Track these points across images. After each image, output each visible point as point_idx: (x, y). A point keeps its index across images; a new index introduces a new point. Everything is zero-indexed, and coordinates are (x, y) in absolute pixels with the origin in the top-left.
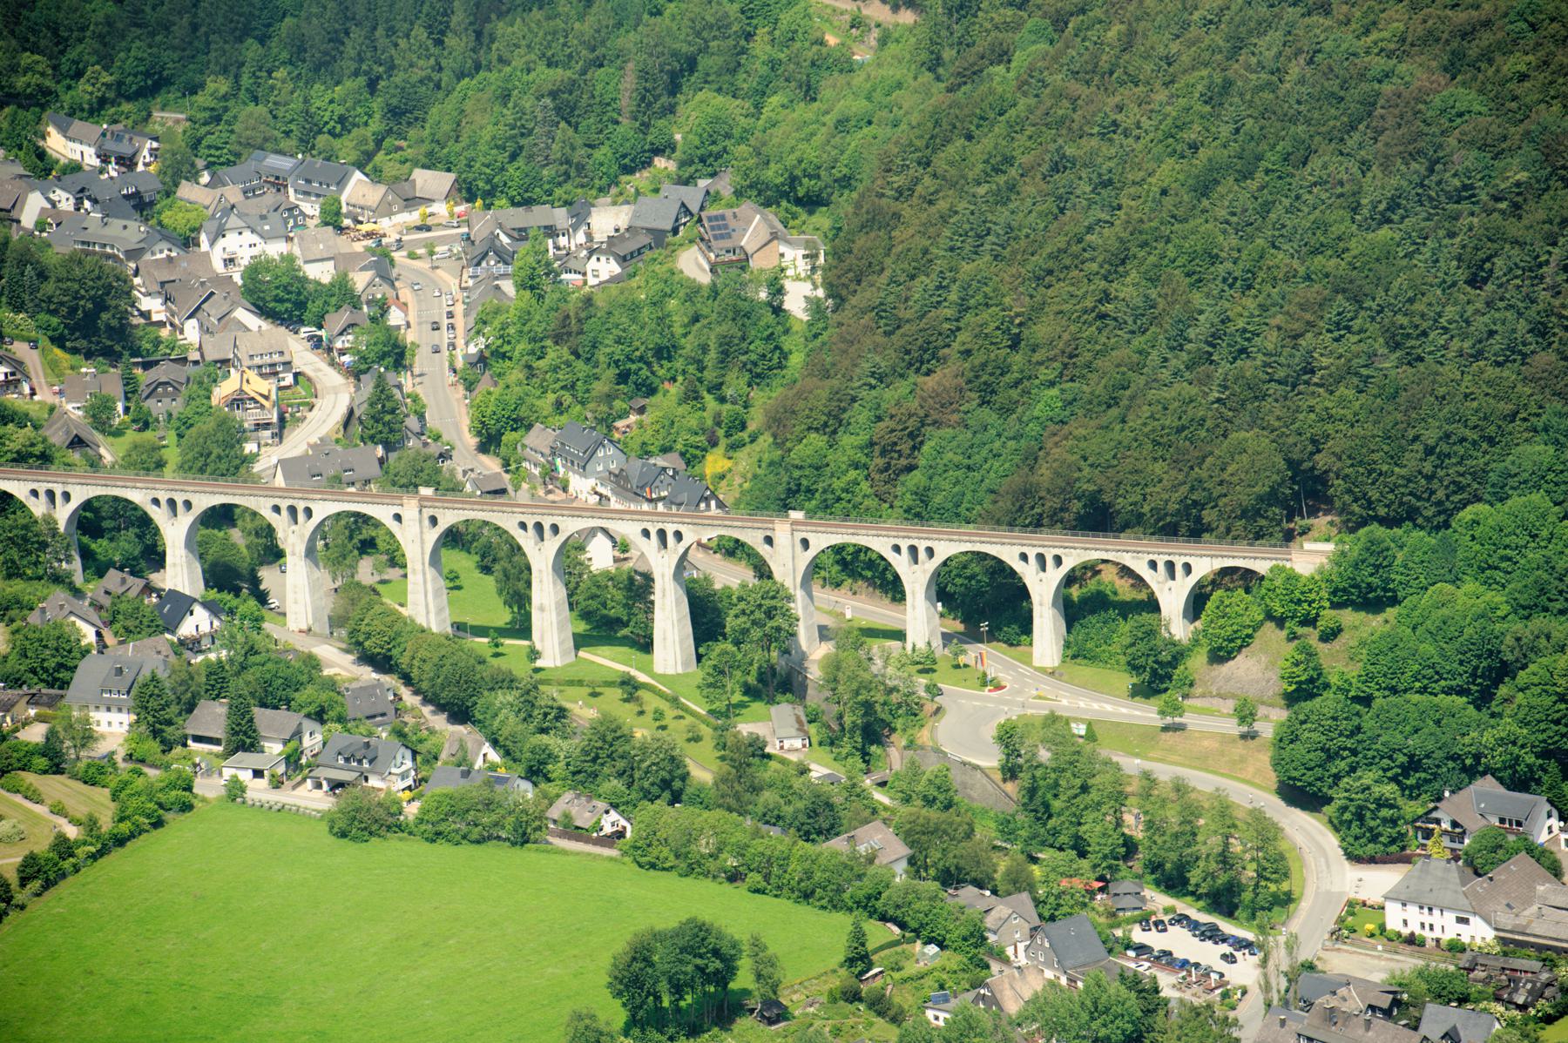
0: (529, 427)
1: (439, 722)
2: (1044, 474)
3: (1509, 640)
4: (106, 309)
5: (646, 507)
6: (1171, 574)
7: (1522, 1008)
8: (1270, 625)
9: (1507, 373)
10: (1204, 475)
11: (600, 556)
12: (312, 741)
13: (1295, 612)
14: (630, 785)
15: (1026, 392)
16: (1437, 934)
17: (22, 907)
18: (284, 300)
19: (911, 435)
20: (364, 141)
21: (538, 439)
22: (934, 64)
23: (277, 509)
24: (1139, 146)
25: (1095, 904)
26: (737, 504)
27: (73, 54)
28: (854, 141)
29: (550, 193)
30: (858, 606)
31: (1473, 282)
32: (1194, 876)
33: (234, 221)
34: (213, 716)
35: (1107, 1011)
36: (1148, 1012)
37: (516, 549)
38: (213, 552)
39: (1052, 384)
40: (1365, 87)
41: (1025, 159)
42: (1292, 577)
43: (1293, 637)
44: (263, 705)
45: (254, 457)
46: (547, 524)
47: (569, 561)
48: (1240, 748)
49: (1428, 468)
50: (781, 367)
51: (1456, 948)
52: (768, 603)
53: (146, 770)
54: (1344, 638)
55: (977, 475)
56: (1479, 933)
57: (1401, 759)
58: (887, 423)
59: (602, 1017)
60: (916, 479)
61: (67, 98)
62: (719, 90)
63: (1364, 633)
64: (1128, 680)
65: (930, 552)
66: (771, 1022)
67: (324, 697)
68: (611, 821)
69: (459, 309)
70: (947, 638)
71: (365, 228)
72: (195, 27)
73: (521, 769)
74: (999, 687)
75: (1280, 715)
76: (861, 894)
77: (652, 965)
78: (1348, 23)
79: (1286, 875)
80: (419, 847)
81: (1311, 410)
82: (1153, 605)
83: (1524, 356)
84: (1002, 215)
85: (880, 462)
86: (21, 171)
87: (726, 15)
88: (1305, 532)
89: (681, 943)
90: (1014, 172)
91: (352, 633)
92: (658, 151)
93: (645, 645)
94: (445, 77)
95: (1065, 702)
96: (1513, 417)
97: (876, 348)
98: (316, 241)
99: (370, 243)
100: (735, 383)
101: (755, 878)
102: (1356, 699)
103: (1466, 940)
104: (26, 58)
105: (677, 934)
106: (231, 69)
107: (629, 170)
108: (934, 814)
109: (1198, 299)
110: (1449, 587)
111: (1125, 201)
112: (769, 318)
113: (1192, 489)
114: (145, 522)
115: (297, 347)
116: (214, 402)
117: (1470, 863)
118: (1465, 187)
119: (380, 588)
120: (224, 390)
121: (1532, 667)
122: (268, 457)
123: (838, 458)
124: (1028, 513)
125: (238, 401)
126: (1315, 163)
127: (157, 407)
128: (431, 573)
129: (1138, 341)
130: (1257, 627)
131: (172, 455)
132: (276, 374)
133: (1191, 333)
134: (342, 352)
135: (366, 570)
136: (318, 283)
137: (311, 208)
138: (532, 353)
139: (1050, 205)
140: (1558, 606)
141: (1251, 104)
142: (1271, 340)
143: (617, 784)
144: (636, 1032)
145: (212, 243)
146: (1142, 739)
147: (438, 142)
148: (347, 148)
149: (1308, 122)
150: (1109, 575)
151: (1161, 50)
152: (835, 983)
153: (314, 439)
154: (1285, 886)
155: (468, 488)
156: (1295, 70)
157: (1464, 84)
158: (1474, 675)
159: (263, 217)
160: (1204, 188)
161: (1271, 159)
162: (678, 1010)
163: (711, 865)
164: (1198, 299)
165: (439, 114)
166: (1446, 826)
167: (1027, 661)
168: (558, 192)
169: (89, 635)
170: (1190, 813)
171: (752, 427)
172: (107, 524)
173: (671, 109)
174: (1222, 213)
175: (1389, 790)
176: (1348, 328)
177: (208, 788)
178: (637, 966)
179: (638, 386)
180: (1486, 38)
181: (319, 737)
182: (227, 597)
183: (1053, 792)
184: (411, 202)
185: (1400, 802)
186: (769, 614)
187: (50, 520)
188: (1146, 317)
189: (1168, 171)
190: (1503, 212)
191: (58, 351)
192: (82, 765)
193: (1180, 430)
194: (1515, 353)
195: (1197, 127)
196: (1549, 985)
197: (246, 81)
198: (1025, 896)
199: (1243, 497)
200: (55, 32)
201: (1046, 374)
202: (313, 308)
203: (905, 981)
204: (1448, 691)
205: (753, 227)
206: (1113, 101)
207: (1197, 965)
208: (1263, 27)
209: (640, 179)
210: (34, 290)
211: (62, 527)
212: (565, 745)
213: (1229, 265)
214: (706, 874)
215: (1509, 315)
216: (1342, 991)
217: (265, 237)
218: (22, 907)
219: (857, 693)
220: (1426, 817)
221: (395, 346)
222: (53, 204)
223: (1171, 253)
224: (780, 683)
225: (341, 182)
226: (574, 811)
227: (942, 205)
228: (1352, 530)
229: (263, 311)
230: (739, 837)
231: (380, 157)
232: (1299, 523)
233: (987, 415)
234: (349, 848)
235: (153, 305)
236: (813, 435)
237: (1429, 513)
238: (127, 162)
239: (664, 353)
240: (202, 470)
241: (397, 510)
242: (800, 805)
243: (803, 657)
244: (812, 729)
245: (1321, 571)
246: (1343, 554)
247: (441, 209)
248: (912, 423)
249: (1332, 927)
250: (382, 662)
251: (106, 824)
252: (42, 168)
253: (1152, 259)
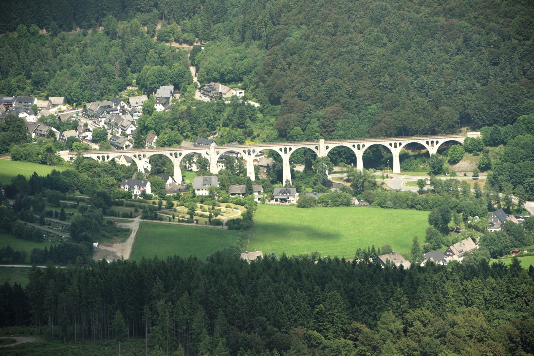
13: (472, 148)
74: (392, 178)
107: (121, 91)
147: (56, 89)
241: (208, 151)
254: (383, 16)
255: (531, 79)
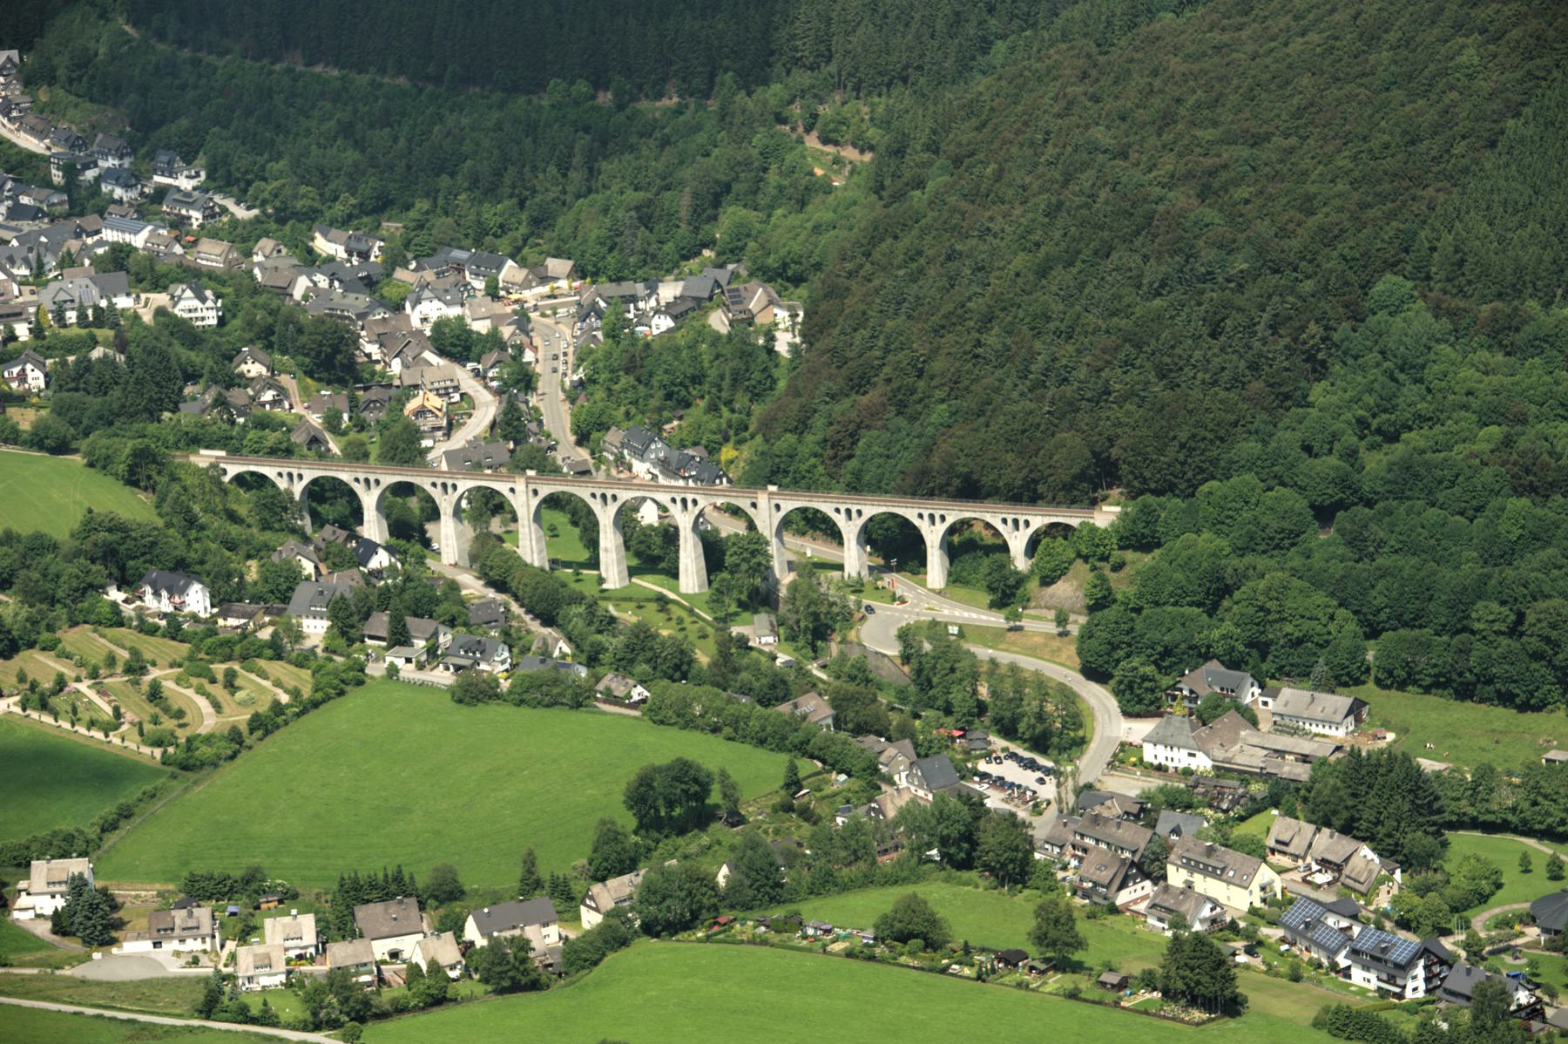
0: (608, 429)
1: (535, 626)
2: (936, 461)
3: (1230, 570)
4: (339, 352)
5: (681, 483)
6: (1017, 528)
7: (1225, 811)
8: (1079, 561)
9: (1233, 395)
10: (1038, 461)
11: (648, 516)
12: (445, 639)
13: (1095, 550)
14: (654, 669)
15: (926, 406)
16: (1175, 764)
17: (250, 748)
18: (455, 343)
19: (851, 435)
20: (516, 240)
21: (613, 437)
22: (878, 189)
23: (434, 485)
24: (1002, 244)
25: (956, 746)
26: (739, 479)
27: (332, 186)
28: (824, 239)
29: (634, 273)
30: (813, 548)
31: (1214, 335)
32: (1022, 727)
33: (427, 293)
34: (381, 622)
35: (949, 818)
36: (977, 819)
37: (590, 512)
38: (396, 513)
39: (943, 401)
40: (1146, 206)
41: (930, 253)
42: (1093, 529)
43: (1094, 569)
44: (416, 615)
45: (429, 449)
46: (609, 494)
47: (626, 518)
48: (1057, 643)
49: (1181, 457)
50: (772, 389)
51: (1187, 772)
52: (753, 547)
53: (336, 658)
54: (1127, 569)
55: (893, 461)
56: (1202, 763)
57: (1159, 649)
58: (836, 427)
59: (620, 822)
60: (853, 464)
61: (327, 214)
62: (745, 206)
63: (1139, 566)
64: (987, 598)
65: (859, 513)
66: (733, 825)
67: (455, 609)
68: (638, 692)
69: (571, 349)
70: (871, 569)
71: (514, 297)
72: (409, 167)
73: (583, 658)
74: (903, 602)
75: (1083, 620)
76: (797, 741)
77: (653, 788)
78: (1138, 164)
79: (1081, 726)
80: (508, 710)
81: (1108, 418)
82: (1004, 548)
83: (1244, 384)
84: (913, 289)
85: (830, 452)
86: (296, 262)
87: (750, 156)
88: (1104, 499)
89: (672, 774)
90: (922, 261)
91: (483, 566)
92: (705, 246)
93: (674, 574)
94: (568, 198)
95: (946, 612)
96: (1235, 424)
97: (830, 378)
98: (480, 306)
99: (516, 307)
100: (741, 400)
101: (728, 730)
102: (1133, 610)
103: (1193, 767)
104: (303, 189)
105: (669, 768)
106: (432, 194)
107: (686, 258)
108: (851, 687)
109: (1038, 345)
110: (1194, 536)
111: (992, 280)
112: (764, 356)
113: (1031, 471)
114: (352, 494)
115: (463, 375)
116: (406, 412)
117: (1200, 717)
118: (1209, 273)
119: (505, 537)
120: (412, 405)
121: (1243, 588)
122: (438, 450)
123: (804, 450)
124: (924, 487)
125: (422, 412)
126: (1115, 256)
127: (370, 417)
128: (534, 526)
129: (999, 373)
130: (1070, 563)
131: (374, 451)
132: (448, 394)
133: (1033, 368)
134: (492, 379)
135: (496, 525)
136: (479, 333)
137: (479, 284)
138: (611, 380)
139: (944, 282)
140: (1261, 548)
141: (1074, 217)
142: (1082, 372)
143: (645, 667)
144: (643, 832)
145: (413, 308)
146: (992, 637)
148: (504, 244)
149: (1111, 229)
150: (978, 528)
151: (1019, 182)
152: (776, 800)
153: (470, 438)
154: (1081, 733)
155: (565, 470)
156: (1103, 194)
157: (1210, 206)
158: (1208, 593)
159: (446, 291)
160: (1043, 272)
161: (1086, 253)
162: (671, 818)
163: (700, 722)
164: (1038, 345)
165: (564, 222)
166: (1186, 693)
167: (923, 584)
168: (639, 272)
169: (308, 567)
170: (1019, 685)
171: (752, 428)
172: (328, 494)
173: (715, 218)
174: (1054, 289)
175: (1149, 670)
176: (1133, 365)
177: (375, 670)
178: (643, 789)
179: (679, 402)
180: (1224, 176)
181: (449, 637)
182: (402, 542)
183: (934, 668)
184: (544, 279)
185: (1158, 677)
186: (753, 553)
187: (289, 493)
188: (1004, 356)
189: (1020, 261)
190: (1232, 290)
191: (309, 380)
192: (294, 654)
193: (1024, 432)
194: (1237, 382)
195: (1040, 232)
196: (1242, 796)
197: (441, 201)
198: (907, 742)
199: (1065, 476)
200: (322, 173)
201: (939, 394)
202: (476, 350)
203: (823, 798)
204: (1191, 604)
205: (757, 298)
206: (988, 214)
207: (1019, 787)
208: (1085, 166)
209: (693, 264)
210: (294, 341)
211: (297, 498)
212: (614, 641)
213: (1058, 323)
214: (696, 728)
215: (1235, 357)
216: (1108, 803)
217: (448, 304)
218: (250, 748)
219: (808, 606)
220: (1174, 687)
221: (526, 375)
222: (315, 284)
223: (1021, 314)
224: (761, 599)
225: (499, 268)
226: (613, 686)
227: (877, 282)
228: (1134, 498)
229: (442, 352)
230: (718, 703)
231: (526, 250)
232: (1101, 493)
233: (902, 422)
234: (464, 710)
235: (373, 350)
236: (788, 435)
237: (1182, 487)
238: (364, 255)
239: (697, 379)
240: (392, 459)
241: (511, 485)
242: (765, 681)
243: (777, 582)
244: (781, 631)
245: (1112, 525)
246: (1127, 514)
247: (563, 284)
248: (852, 427)
249: (1109, 759)
250: (500, 586)
251: (307, 692)
252: (311, 261)
253: (1009, 319)
254: (1171, 371)
255: (1271, 386)
